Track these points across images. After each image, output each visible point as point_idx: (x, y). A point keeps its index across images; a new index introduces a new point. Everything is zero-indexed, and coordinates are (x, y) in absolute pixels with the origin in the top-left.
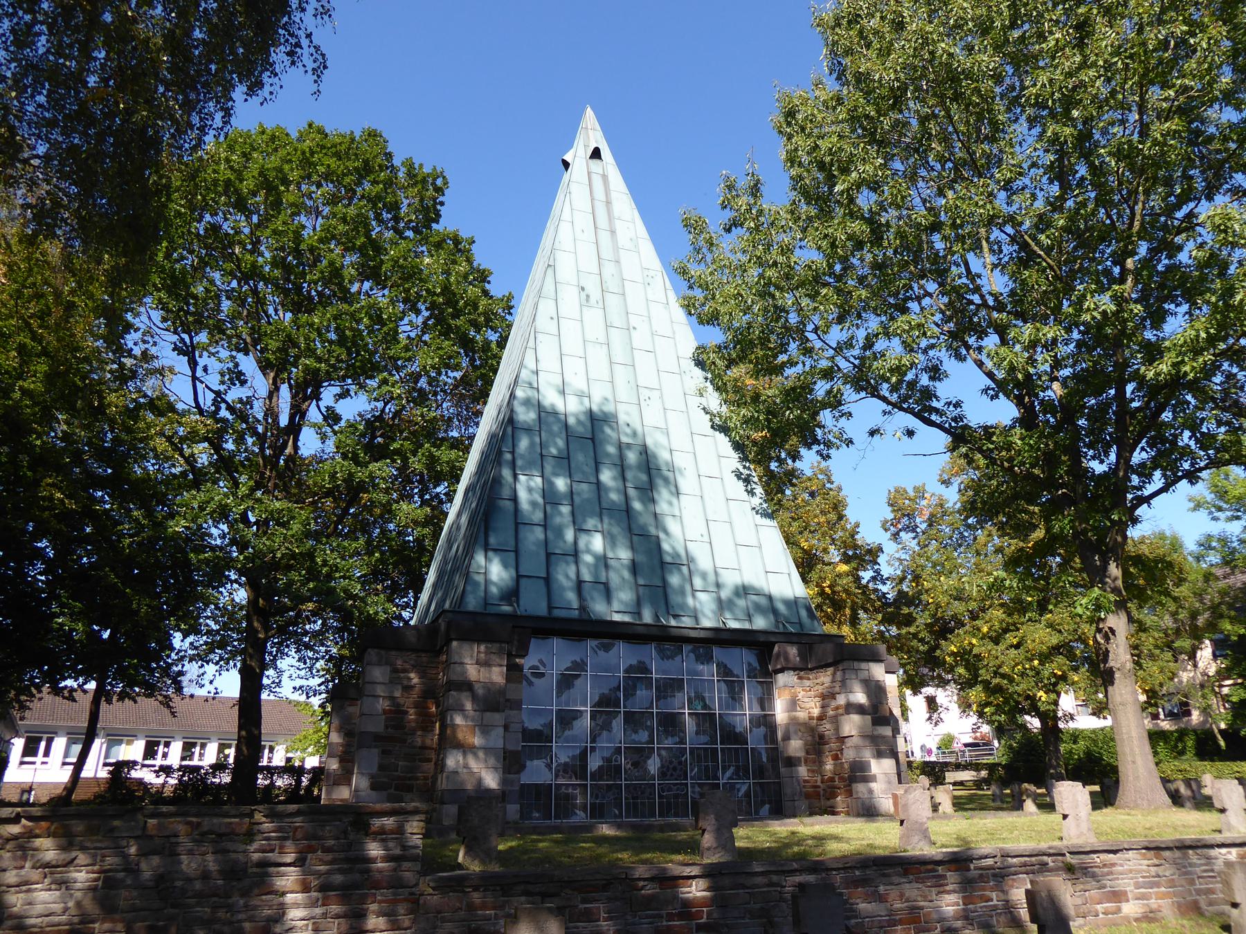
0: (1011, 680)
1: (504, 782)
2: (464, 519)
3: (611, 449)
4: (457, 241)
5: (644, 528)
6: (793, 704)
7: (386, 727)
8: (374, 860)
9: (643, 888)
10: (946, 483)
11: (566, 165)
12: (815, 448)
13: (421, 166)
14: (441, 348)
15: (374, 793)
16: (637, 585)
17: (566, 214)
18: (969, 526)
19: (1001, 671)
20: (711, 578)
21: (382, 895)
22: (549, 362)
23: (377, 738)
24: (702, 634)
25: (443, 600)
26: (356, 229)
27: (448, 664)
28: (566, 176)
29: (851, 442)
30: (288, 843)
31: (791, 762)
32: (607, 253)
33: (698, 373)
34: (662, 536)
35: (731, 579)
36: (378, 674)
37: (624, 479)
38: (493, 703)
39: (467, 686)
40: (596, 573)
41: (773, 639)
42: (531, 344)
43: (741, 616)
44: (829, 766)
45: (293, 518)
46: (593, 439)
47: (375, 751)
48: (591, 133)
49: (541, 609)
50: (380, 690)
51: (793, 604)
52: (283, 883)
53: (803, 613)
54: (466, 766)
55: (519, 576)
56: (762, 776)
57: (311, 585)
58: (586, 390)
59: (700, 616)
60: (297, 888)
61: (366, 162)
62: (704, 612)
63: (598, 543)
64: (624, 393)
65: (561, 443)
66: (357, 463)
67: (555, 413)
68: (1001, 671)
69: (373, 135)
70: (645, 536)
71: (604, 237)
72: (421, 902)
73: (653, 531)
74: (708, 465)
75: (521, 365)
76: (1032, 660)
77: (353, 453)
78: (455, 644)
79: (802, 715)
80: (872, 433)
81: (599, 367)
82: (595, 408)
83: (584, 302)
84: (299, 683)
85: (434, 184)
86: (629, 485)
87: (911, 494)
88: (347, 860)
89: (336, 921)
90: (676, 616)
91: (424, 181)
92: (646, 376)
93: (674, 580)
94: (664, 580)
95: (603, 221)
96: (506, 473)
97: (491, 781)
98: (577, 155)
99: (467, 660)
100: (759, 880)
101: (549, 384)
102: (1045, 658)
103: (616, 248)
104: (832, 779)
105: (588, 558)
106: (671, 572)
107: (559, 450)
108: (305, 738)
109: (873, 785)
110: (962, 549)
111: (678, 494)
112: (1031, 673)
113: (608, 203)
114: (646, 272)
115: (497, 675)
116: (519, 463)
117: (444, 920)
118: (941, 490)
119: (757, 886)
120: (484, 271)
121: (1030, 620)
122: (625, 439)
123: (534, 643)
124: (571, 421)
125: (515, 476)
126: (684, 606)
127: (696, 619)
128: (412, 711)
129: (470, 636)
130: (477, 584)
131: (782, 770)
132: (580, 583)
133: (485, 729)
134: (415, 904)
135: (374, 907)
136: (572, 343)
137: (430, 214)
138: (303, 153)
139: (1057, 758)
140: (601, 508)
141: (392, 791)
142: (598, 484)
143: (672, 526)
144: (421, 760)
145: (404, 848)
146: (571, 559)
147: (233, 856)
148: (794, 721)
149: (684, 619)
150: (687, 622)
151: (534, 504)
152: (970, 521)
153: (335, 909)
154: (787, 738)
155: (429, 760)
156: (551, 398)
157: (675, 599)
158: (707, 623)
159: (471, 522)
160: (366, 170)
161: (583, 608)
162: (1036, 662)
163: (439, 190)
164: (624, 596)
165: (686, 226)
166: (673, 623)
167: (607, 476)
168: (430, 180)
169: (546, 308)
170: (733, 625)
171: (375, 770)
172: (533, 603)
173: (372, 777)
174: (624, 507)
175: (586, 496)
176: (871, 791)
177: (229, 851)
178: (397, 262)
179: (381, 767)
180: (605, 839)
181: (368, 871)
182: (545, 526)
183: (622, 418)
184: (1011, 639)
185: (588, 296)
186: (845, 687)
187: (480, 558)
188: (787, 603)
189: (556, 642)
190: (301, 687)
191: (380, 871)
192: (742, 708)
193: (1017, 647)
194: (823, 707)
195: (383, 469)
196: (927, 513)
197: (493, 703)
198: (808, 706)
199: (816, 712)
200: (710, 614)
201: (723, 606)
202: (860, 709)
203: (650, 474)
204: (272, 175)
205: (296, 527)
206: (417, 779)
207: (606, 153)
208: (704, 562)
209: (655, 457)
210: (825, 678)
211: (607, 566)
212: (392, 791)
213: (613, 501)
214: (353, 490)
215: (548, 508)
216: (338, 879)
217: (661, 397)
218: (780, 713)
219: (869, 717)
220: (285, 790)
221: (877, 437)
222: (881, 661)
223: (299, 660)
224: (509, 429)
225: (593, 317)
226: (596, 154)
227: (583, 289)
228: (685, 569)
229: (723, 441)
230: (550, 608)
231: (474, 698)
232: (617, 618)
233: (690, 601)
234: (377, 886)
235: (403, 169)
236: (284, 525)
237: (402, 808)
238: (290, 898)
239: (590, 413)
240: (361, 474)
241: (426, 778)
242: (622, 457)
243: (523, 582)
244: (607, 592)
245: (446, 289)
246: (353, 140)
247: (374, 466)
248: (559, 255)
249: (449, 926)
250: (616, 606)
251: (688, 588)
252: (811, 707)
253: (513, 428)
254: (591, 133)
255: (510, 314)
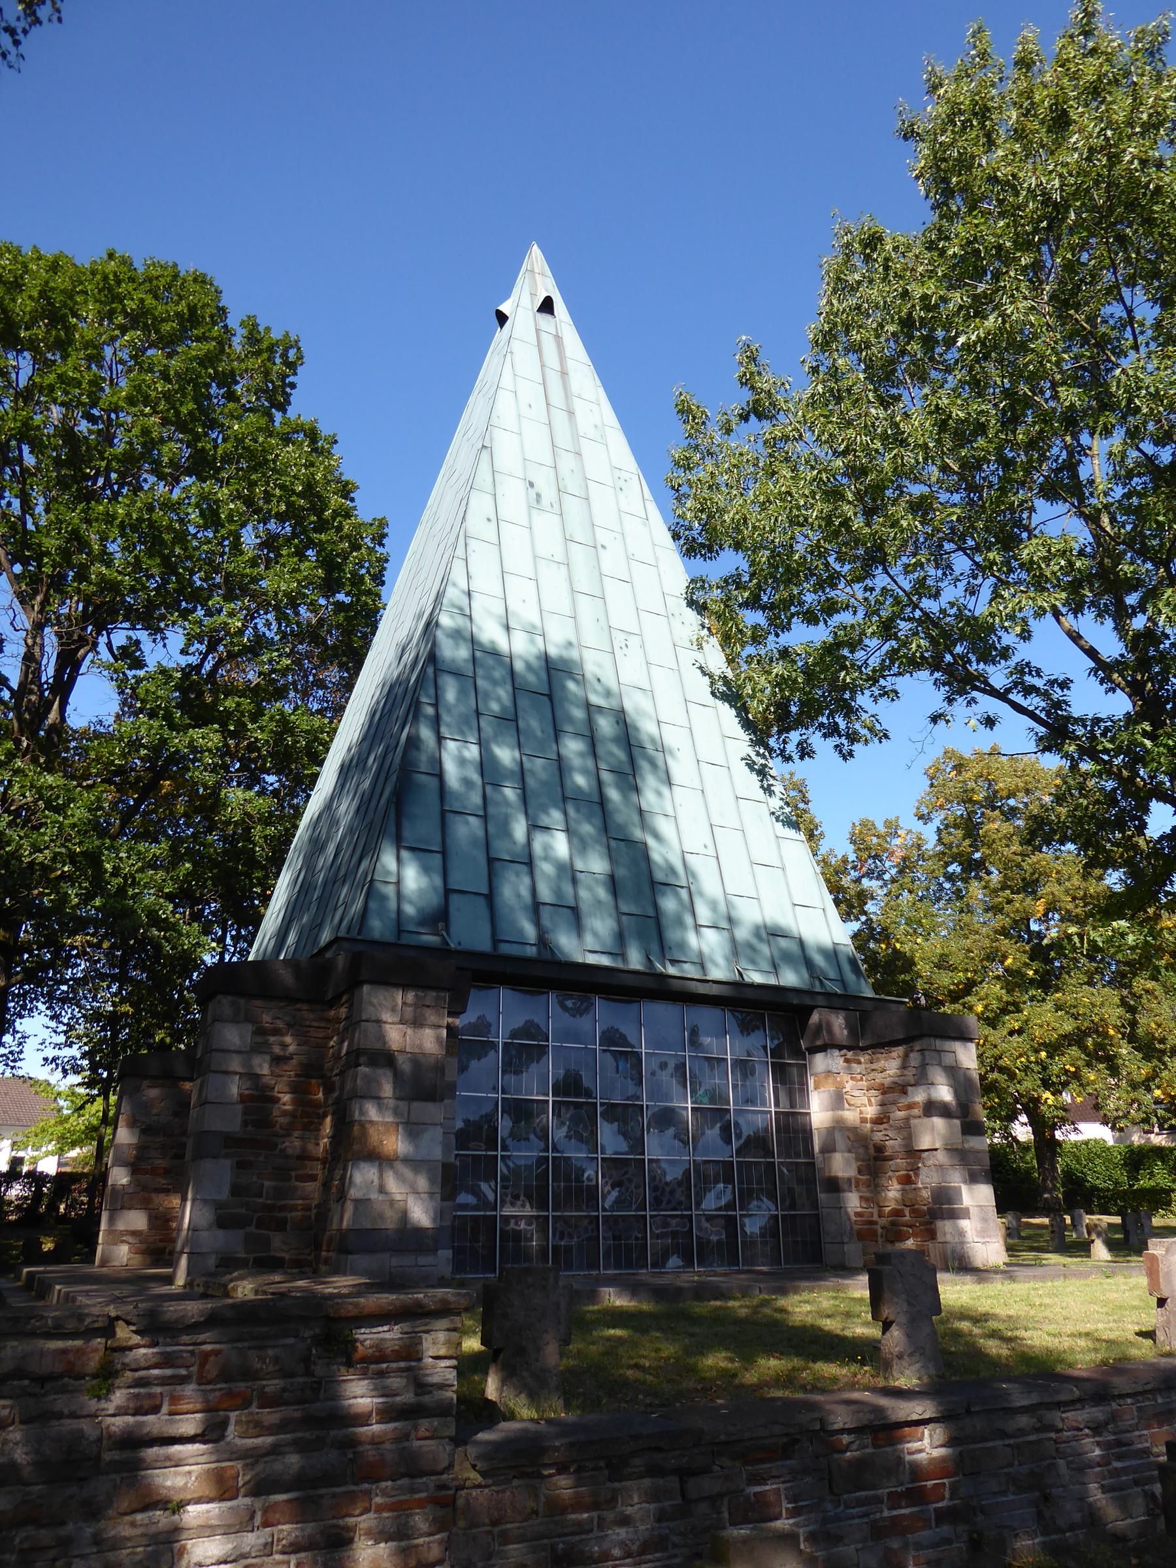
0: (1012, 1076)
1: (440, 1214)
2: (346, 808)
3: (578, 713)
4: (313, 435)
5: (622, 828)
6: (838, 1100)
7: (245, 1123)
8: (362, 1419)
9: (847, 1448)
10: (924, 818)
11: (502, 318)
12: (835, 740)
13: (268, 329)
14: (299, 570)
15: (220, 1233)
16: (619, 914)
17: (507, 380)
18: (950, 878)
19: (1001, 1062)
20: (722, 908)
21: (384, 1493)
22: (485, 581)
23: (230, 1141)
24: (715, 990)
25: (316, 927)
26: (182, 389)
27: (353, 1022)
28: (501, 335)
29: (886, 736)
30: (190, 1389)
31: (834, 1186)
32: (563, 440)
33: (691, 616)
34: (651, 842)
35: (750, 915)
36: (233, 1036)
37: (595, 755)
38: (422, 1086)
39: (385, 1058)
40: (558, 892)
41: (808, 1001)
42: (460, 552)
43: (765, 966)
44: (893, 1193)
45: (73, 800)
46: (550, 697)
47: (227, 1163)
48: (536, 277)
49: (483, 943)
50: (235, 1064)
51: (833, 954)
52: (180, 1482)
53: (846, 968)
54: (382, 1189)
55: (448, 892)
56: (793, 1206)
57: (98, 902)
58: (538, 623)
59: (709, 966)
60: (207, 1491)
61: (192, 309)
62: (708, 953)
63: (560, 845)
64: (592, 636)
65: (504, 693)
66: (172, 726)
67: (494, 653)
68: (1001, 1062)
69: (201, 280)
70: (629, 842)
71: (560, 418)
72: (460, 1502)
73: (638, 834)
74: (710, 749)
75: (445, 580)
76: (1037, 1051)
77: (166, 709)
78: (366, 988)
79: (850, 1116)
80: (935, 719)
81: (557, 597)
82: (553, 652)
83: (534, 504)
84: (51, 1053)
85: (284, 355)
86: (602, 766)
87: (881, 829)
88: (310, 1421)
89: (293, 1560)
90: (674, 962)
91: (271, 349)
92: (621, 616)
93: (669, 904)
94: (656, 906)
95: (557, 398)
96: (426, 733)
97: (421, 1214)
98: (520, 305)
99: (386, 1016)
100: (1024, 1421)
101: (489, 613)
102: (1054, 1049)
103: (576, 435)
104: (897, 1213)
105: (546, 868)
106: (664, 894)
107: (504, 708)
108: (43, 1131)
109: (964, 1224)
110: (942, 904)
111: (669, 783)
112: (1037, 1068)
113: (564, 374)
114: (617, 473)
115: (429, 1040)
116: (446, 718)
117: (505, 1539)
118: (918, 826)
119: (1022, 1432)
120: (347, 483)
121: (1032, 999)
122: (595, 699)
123: (474, 994)
124: (519, 666)
125: (440, 739)
126: (682, 946)
127: (702, 966)
128: (286, 1098)
129: (388, 979)
130: (384, 898)
131: (822, 1196)
132: (536, 907)
133: (413, 1129)
134: (447, 1506)
135: (365, 1521)
136: (518, 558)
137: (277, 396)
138: (105, 278)
139: (1054, 1179)
140: (565, 797)
141: (252, 1229)
142: (560, 759)
143: (664, 826)
144: (300, 1178)
145: (421, 1386)
146: (524, 868)
147: (70, 1424)
148: (838, 1126)
149: (686, 966)
150: (690, 971)
151: (467, 782)
152: (950, 869)
153: (287, 1530)
154: (829, 1149)
155: (313, 1178)
156: (490, 632)
157: (672, 935)
158: (719, 972)
159: (362, 810)
160: (192, 318)
161: (543, 941)
162: (1043, 1054)
163: (292, 366)
164: (601, 926)
165: (681, 412)
166: (672, 970)
167: (573, 747)
168: (280, 350)
169: (480, 505)
170: (756, 978)
171: (224, 1195)
172: (469, 932)
173: (218, 1206)
174: (596, 799)
175: (543, 776)
176: (962, 1234)
177: (59, 1416)
178: (242, 441)
179: (236, 1190)
180: (618, 1318)
181: (352, 1443)
182: (485, 818)
183: (590, 669)
184: (1012, 1022)
185: (538, 495)
186: (922, 1079)
187: (388, 860)
188: (823, 951)
189: (504, 995)
190: (54, 1059)
191: (376, 1441)
192: (764, 1104)
193: (1020, 1032)
194: (882, 1104)
195: (209, 737)
196: (900, 853)
197: (422, 1086)
198: (858, 1102)
199: (871, 1111)
200: (721, 961)
201: (736, 949)
202: (943, 1110)
203: (631, 754)
204: (58, 299)
205: (78, 812)
206: (293, 1208)
207: (559, 305)
208: (709, 884)
209: (637, 729)
210: (890, 1066)
211: (574, 881)
212: (252, 1229)
213: (579, 788)
214: (165, 763)
215: (489, 789)
216: (293, 1461)
217: (643, 646)
218: (818, 1112)
219: (957, 1122)
220: (18, 1208)
221: (942, 723)
222: (971, 1040)
223: (52, 1018)
224: (430, 671)
225: (546, 524)
226: (547, 306)
227: (531, 485)
228: (684, 893)
229: (727, 713)
230: (496, 941)
231: (398, 1077)
232: (592, 959)
233: (692, 939)
234: (372, 1474)
235: (241, 333)
236: (58, 810)
237: (418, 1304)
238: (194, 1513)
239: (546, 658)
240: (178, 742)
241: (307, 1208)
242: (590, 721)
243: (454, 898)
244: (575, 916)
245: (310, 486)
246: (176, 276)
247: (196, 733)
248: (497, 433)
249: (515, 1551)
250: (590, 941)
251: (689, 920)
252: (862, 1107)
253: (436, 670)
254: (536, 277)
255: (381, 545)
